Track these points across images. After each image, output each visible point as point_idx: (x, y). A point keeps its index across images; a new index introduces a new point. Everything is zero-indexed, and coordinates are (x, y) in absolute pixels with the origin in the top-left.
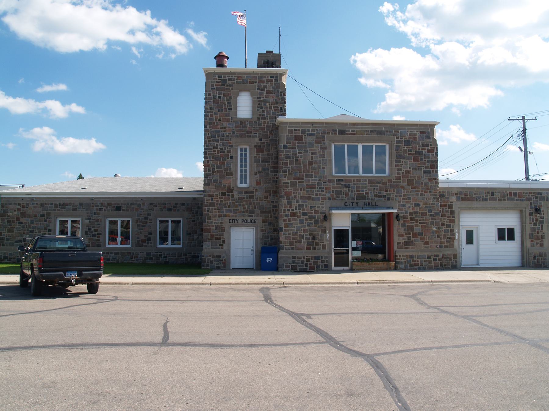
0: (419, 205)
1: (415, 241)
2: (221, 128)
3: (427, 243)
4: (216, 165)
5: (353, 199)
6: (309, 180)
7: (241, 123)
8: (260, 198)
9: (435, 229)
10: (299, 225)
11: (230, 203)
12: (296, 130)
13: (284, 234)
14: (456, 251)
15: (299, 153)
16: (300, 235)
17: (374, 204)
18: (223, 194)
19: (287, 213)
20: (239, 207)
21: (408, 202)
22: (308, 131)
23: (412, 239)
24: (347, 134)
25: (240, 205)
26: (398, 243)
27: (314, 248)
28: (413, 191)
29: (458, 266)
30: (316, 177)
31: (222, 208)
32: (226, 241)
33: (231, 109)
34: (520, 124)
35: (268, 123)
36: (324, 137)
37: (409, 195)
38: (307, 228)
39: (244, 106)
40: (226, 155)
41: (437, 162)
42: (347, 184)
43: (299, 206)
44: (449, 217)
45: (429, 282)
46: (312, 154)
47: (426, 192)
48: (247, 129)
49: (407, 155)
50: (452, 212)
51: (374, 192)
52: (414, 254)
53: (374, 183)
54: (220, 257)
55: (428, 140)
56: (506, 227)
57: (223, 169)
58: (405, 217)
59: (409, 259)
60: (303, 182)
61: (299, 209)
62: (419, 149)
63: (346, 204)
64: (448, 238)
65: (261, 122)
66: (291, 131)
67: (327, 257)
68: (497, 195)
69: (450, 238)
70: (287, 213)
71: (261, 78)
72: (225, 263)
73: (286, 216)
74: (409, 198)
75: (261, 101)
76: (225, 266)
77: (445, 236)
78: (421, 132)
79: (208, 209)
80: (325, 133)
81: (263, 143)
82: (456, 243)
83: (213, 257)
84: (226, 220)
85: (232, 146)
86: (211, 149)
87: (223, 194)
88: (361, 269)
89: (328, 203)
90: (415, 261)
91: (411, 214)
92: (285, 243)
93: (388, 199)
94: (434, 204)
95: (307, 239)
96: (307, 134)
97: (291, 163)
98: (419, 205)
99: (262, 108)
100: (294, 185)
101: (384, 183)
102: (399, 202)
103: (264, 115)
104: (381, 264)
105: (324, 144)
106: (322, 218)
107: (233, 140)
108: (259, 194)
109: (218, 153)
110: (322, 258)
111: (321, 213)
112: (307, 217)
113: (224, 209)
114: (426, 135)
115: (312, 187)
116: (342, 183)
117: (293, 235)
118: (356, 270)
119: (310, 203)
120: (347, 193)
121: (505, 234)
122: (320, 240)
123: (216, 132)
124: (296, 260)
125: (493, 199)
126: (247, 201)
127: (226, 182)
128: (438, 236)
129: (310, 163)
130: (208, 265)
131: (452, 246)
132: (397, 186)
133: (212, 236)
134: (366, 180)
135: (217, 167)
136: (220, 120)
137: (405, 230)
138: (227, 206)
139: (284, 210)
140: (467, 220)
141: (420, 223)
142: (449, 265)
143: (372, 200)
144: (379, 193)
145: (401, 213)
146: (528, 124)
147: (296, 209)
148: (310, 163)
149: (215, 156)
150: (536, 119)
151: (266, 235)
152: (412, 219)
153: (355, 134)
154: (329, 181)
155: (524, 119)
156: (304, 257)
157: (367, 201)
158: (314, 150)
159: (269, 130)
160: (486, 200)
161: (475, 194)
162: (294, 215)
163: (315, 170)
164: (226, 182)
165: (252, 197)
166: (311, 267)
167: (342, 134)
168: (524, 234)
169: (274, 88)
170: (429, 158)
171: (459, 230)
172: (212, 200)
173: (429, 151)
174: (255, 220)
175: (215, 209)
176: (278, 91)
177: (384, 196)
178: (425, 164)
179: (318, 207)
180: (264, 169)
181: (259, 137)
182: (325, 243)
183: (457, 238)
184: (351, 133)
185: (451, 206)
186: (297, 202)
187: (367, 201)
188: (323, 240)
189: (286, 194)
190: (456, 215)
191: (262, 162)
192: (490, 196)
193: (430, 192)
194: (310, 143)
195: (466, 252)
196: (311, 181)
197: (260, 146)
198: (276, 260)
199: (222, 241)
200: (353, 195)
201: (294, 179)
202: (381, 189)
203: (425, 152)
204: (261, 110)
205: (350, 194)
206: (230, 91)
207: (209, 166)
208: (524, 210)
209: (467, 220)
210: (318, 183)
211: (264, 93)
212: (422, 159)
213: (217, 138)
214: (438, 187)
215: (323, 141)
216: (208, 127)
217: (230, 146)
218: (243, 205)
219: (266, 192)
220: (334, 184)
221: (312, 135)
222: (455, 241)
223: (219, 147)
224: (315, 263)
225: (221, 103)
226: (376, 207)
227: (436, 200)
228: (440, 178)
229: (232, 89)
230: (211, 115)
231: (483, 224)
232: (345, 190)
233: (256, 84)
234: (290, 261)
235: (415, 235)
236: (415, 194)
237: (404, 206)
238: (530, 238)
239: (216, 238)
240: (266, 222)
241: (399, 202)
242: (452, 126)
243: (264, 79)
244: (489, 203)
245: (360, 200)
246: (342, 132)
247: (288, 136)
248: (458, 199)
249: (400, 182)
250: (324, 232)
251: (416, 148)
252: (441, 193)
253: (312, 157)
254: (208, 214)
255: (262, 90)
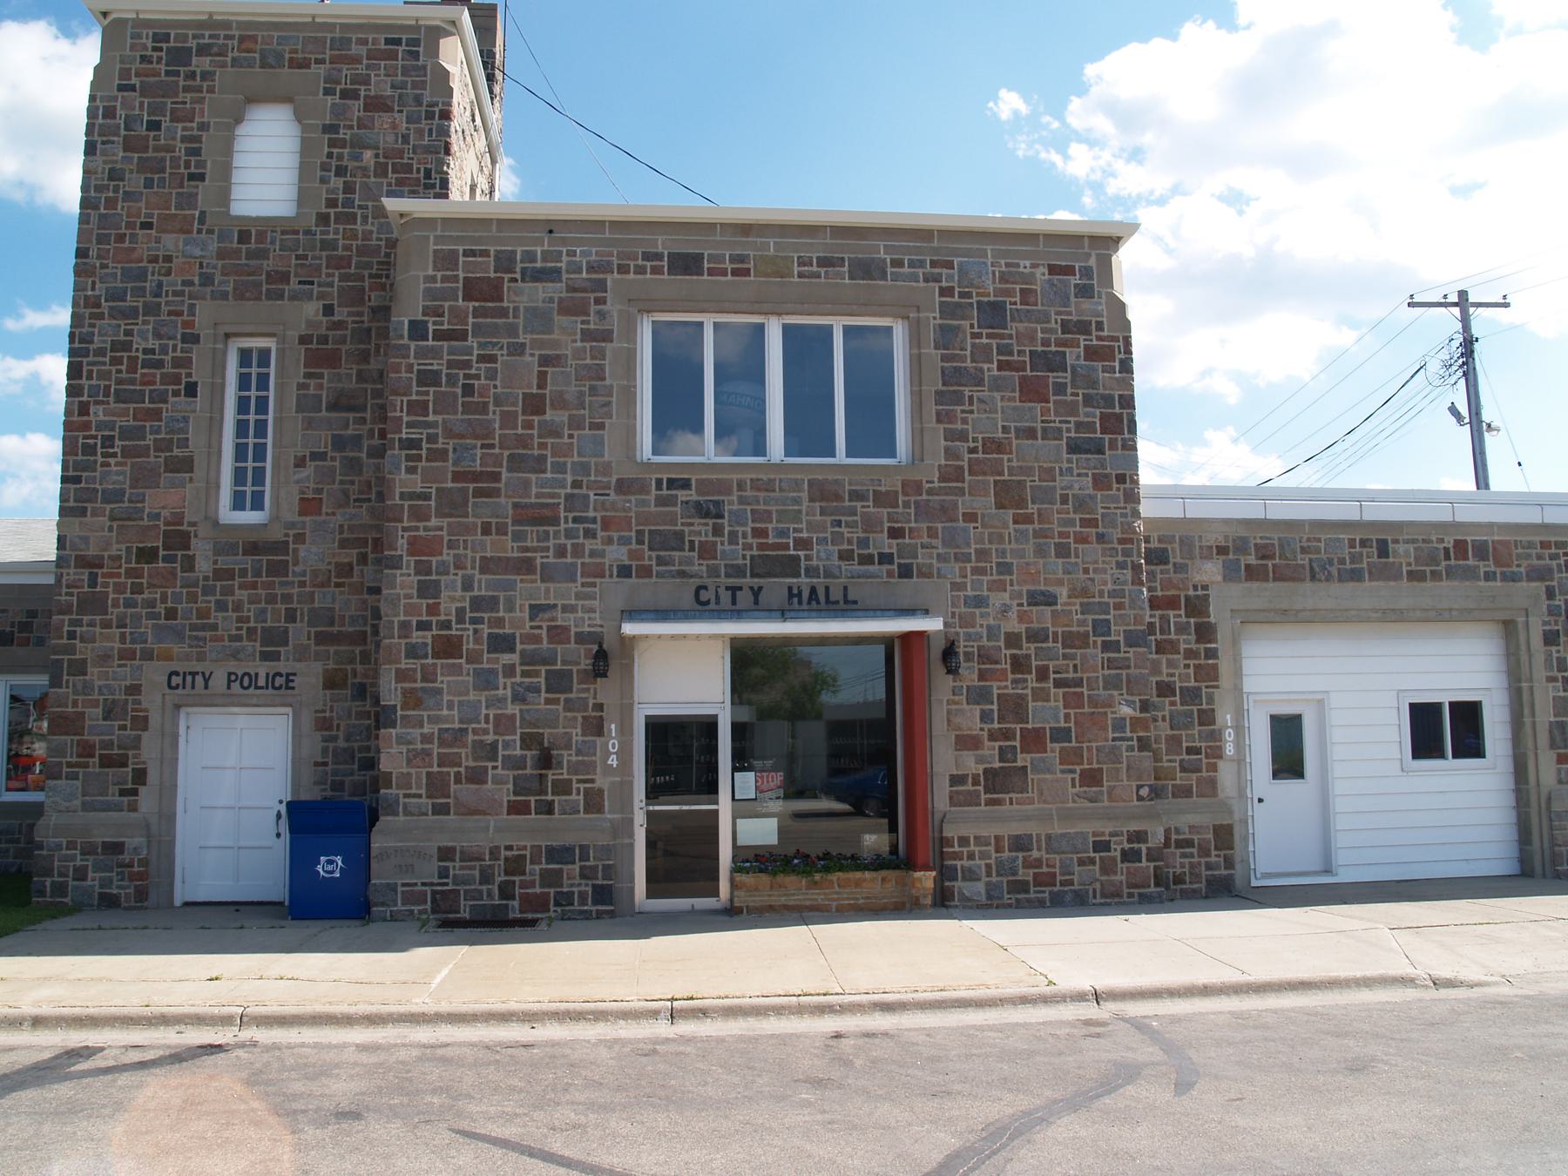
0: (1050, 600)
1: (1036, 770)
2: (154, 260)
3: (1091, 778)
4: (121, 422)
5: (738, 571)
6: (526, 484)
7: (244, 237)
8: (315, 573)
9: (1126, 711)
10: (472, 696)
11: (177, 598)
12: (472, 253)
13: (401, 740)
14: (1231, 812)
15: (482, 359)
16: (478, 745)
17: (836, 594)
18: (147, 555)
19: (417, 637)
20: (217, 617)
21: (999, 586)
22: (530, 257)
23: (1022, 760)
24: (711, 272)
25: (221, 606)
26: (956, 780)
27: (548, 809)
28: (1021, 537)
29: (1238, 882)
30: (560, 468)
31: (137, 617)
32: (152, 776)
33: (201, 177)
34: (1449, 319)
35: (367, 235)
36: (601, 286)
37: (1003, 553)
38: (512, 709)
39: (265, 167)
40: (167, 380)
41: (1128, 402)
42: (707, 499)
43: (477, 604)
44: (1190, 654)
45: (1080, 997)
46: (545, 361)
47: (1083, 540)
48: (268, 265)
49: (991, 369)
50: (1205, 632)
51: (837, 538)
52: (1033, 829)
53: (839, 498)
54: (117, 848)
55: (1086, 305)
56: (1445, 699)
57: (149, 440)
58: (985, 657)
59: (1006, 854)
60: (495, 493)
61: (474, 621)
62: (1046, 343)
63: (704, 596)
64: (1190, 751)
65: (335, 232)
66: (446, 260)
67: (607, 851)
68: (1403, 554)
69: (1197, 751)
70: (417, 637)
71: (345, 42)
72: (141, 876)
73: (413, 652)
74: (1005, 568)
75: (342, 144)
76: (142, 895)
77: (1174, 742)
78: (1053, 270)
79: (73, 623)
80: (604, 267)
81: (339, 325)
82: (1226, 775)
83: (88, 850)
84: (154, 674)
85: (195, 339)
86: (101, 352)
87: (147, 555)
88: (771, 908)
89: (617, 591)
90: (1038, 863)
91: (1012, 640)
92: (405, 781)
93: (905, 572)
94: (1121, 594)
95: (515, 763)
96: (524, 271)
97: (445, 404)
98: (1050, 600)
99: (341, 171)
100: (452, 505)
101: (881, 499)
102: (956, 587)
103: (348, 203)
104: (873, 883)
105: (602, 315)
106: (586, 664)
107: (205, 314)
108: (313, 554)
109: (132, 369)
110: (584, 856)
111: (581, 638)
112: (514, 658)
113: (147, 626)
114: (1075, 280)
115: (542, 517)
116: (682, 495)
117: (442, 743)
118: (750, 910)
119: (528, 590)
120: (700, 547)
121: (1441, 731)
122: (574, 769)
123: (127, 275)
124: (455, 868)
125: (1385, 572)
126: (254, 586)
127: (161, 500)
128: (1144, 744)
129: (535, 405)
130: (60, 889)
131: (1211, 787)
132: (947, 512)
133: (86, 750)
134: (797, 485)
135: (126, 434)
136: (147, 226)
137: (986, 717)
138: (160, 609)
139: (405, 626)
140: (1274, 671)
141: (1058, 684)
142: (1196, 877)
143: (828, 574)
144: (864, 543)
145: (969, 637)
146: (1479, 317)
147: (460, 620)
148: (535, 405)
149: (119, 382)
150: (1506, 305)
151: (341, 743)
152: (1019, 665)
153: (747, 272)
154: (623, 487)
155: (1463, 301)
156: (494, 853)
157: (803, 580)
158: (556, 344)
159: (368, 265)
160: (1356, 576)
161: (1304, 550)
162: (448, 648)
163: (559, 435)
164: (161, 500)
165: (278, 569)
166: (529, 902)
167: (687, 270)
168: (1528, 729)
169: (403, 86)
170: (1093, 384)
171: (1240, 713)
172: (93, 583)
173: (1091, 354)
174: (289, 678)
175: (106, 625)
176: (418, 100)
177: (885, 559)
178: (1074, 413)
179: (565, 609)
180: (339, 443)
181: (321, 296)
182: (602, 782)
183: (1229, 749)
184: (729, 266)
185: (1197, 606)
186: (467, 585)
187: (803, 580)
188: (590, 767)
189: (415, 547)
190: (1222, 643)
191: (333, 407)
192: (1370, 556)
193: (1101, 538)
194: (533, 312)
195: (1275, 820)
196: (537, 488)
197: (324, 340)
198: (361, 864)
199: (127, 768)
200: (739, 554)
201: (457, 477)
202: (870, 524)
203: (1073, 356)
204: (337, 183)
205: (723, 546)
206: (201, 101)
207: (86, 426)
208: (1521, 620)
209: (1274, 671)
210: (569, 497)
211: (356, 108)
212: (1060, 389)
213: (130, 301)
214: (1136, 514)
215: (598, 301)
216: (93, 253)
217: (186, 339)
218: (238, 607)
219: (344, 544)
220: (644, 503)
221: (550, 275)
222: (1221, 764)
223: (138, 343)
224: (551, 878)
225: (156, 149)
226: (847, 606)
227: (1128, 573)
228: (1147, 477)
229: (211, 90)
230: (111, 203)
231: (1346, 684)
232: (700, 530)
233: (322, 70)
234: (428, 871)
235: (1034, 740)
236: (1029, 548)
237: (980, 602)
238: (1553, 746)
239: (107, 762)
240: (343, 685)
241: (956, 587)
242: (1209, 434)
243: (355, 50)
244: (1370, 593)
245: (773, 576)
246: (686, 264)
247: (433, 279)
248: (1230, 574)
249: (961, 492)
250: (596, 728)
251: (1032, 338)
252: (1154, 545)
253: (542, 376)
254: (71, 650)
255: (345, 95)
